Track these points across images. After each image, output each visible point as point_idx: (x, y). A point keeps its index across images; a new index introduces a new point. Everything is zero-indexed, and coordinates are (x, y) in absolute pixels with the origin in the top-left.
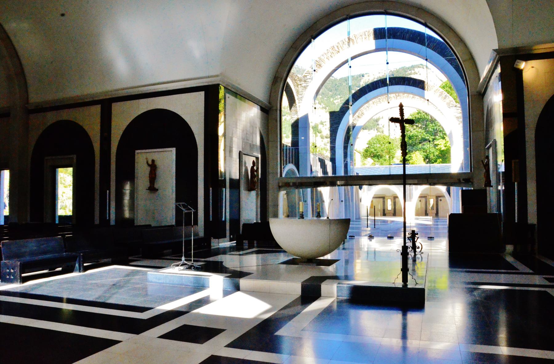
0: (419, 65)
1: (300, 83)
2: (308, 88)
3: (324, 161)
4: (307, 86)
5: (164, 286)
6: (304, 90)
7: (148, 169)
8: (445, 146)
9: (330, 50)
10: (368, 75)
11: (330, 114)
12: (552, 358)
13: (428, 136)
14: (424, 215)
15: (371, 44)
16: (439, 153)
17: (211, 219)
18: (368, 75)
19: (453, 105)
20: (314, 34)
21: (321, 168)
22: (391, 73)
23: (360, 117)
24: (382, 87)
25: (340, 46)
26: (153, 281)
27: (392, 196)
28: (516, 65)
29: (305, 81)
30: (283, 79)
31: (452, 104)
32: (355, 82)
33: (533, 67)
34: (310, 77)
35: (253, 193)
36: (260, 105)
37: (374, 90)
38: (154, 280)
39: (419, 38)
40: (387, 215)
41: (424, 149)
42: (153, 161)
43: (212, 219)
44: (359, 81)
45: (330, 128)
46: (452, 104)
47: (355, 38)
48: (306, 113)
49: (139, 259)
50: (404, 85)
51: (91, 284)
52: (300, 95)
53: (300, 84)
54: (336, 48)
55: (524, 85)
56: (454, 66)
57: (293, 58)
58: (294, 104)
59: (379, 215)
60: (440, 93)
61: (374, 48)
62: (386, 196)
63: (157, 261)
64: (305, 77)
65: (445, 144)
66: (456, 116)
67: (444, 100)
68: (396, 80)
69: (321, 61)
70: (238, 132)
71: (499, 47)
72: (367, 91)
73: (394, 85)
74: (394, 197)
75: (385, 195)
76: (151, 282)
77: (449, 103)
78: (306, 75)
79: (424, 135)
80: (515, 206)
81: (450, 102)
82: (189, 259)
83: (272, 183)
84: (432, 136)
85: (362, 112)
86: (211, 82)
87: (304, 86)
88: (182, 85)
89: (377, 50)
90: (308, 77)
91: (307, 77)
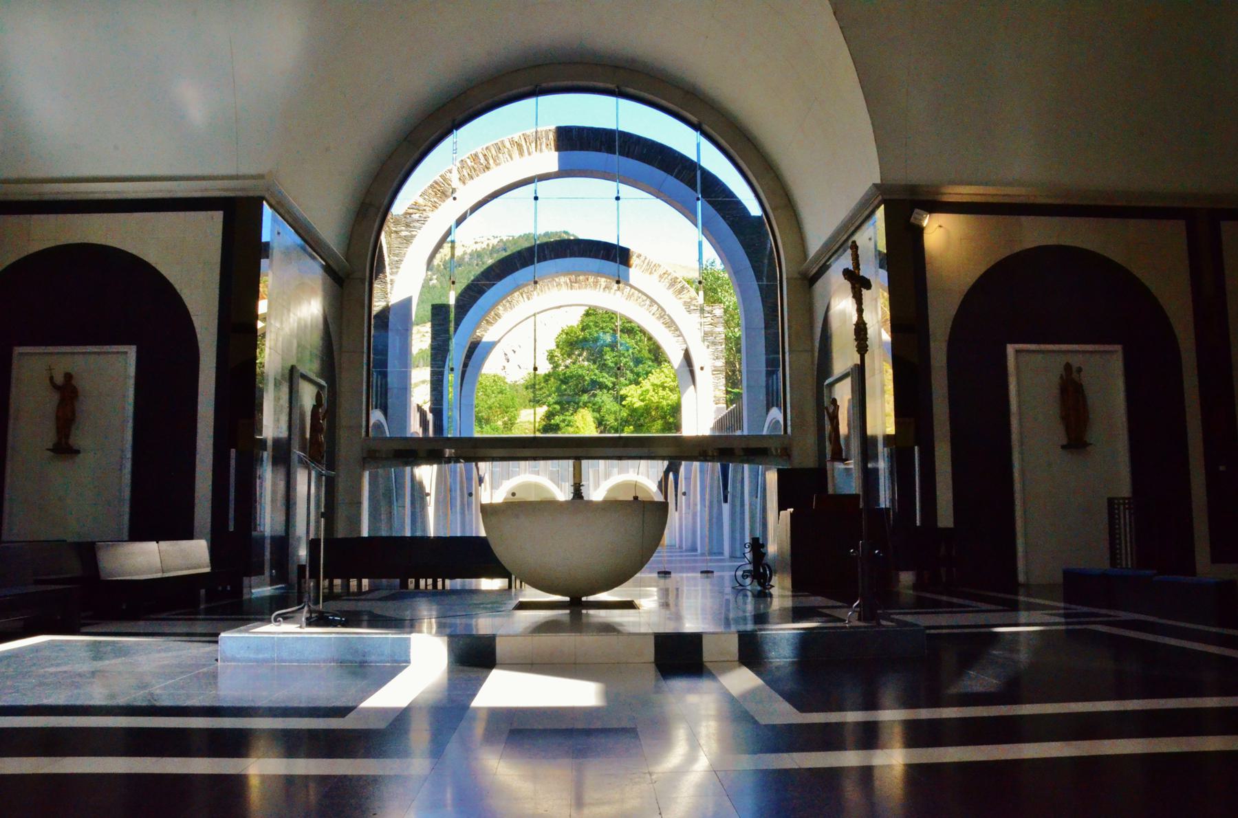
0: (560, 232)
1: (394, 229)
2: (415, 241)
4: (413, 236)
5: (273, 668)
6: (405, 245)
7: (55, 398)
8: (642, 400)
9: (468, 161)
11: (432, 309)
12: (1235, 748)
13: (603, 377)
15: (550, 160)
16: (629, 415)
17: (233, 527)
20: (460, 118)
21: (421, 426)
22: (501, 244)
23: (491, 323)
24: (551, 259)
25: (490, 155)
26: (238, 656)
28: (915, 218)
29: (407, 225)
31: (694, 305)
33: (940, 226)
34: (420, 216)
38: (243, 654)
41: (594, 404)
42: (68, 377)
47: (526, 142)
48: (410, 295)
49: (89, 622)
51: (55, 674)
52: (395, 255)
53: (396, 232)
54: (482, 160)
55: (926, 256)
56: (728, 221)
58: (381, 276)
60: (671, 280)
61: (554, 168)
63: (142, 623)
64: (408, 216)
65: (642, 395)
67: (680, 296)
68: (582, 246)
69: (446, 184)
70: (291, 320)
71: (881, 180)
72: (518, 265)
76: (234, 659)
77: (689, 303)
78: (411, 211)
79: (595, 375)
80: (915, 498)
81: (689, 300)
82: (240, 617)
83: (348, 448)
84: (611, 376)
86: (234, 190)
87: (405, 236)
88: (161, 191)
89: (563, 173)
90: (416, 217)
91: (412, 216)
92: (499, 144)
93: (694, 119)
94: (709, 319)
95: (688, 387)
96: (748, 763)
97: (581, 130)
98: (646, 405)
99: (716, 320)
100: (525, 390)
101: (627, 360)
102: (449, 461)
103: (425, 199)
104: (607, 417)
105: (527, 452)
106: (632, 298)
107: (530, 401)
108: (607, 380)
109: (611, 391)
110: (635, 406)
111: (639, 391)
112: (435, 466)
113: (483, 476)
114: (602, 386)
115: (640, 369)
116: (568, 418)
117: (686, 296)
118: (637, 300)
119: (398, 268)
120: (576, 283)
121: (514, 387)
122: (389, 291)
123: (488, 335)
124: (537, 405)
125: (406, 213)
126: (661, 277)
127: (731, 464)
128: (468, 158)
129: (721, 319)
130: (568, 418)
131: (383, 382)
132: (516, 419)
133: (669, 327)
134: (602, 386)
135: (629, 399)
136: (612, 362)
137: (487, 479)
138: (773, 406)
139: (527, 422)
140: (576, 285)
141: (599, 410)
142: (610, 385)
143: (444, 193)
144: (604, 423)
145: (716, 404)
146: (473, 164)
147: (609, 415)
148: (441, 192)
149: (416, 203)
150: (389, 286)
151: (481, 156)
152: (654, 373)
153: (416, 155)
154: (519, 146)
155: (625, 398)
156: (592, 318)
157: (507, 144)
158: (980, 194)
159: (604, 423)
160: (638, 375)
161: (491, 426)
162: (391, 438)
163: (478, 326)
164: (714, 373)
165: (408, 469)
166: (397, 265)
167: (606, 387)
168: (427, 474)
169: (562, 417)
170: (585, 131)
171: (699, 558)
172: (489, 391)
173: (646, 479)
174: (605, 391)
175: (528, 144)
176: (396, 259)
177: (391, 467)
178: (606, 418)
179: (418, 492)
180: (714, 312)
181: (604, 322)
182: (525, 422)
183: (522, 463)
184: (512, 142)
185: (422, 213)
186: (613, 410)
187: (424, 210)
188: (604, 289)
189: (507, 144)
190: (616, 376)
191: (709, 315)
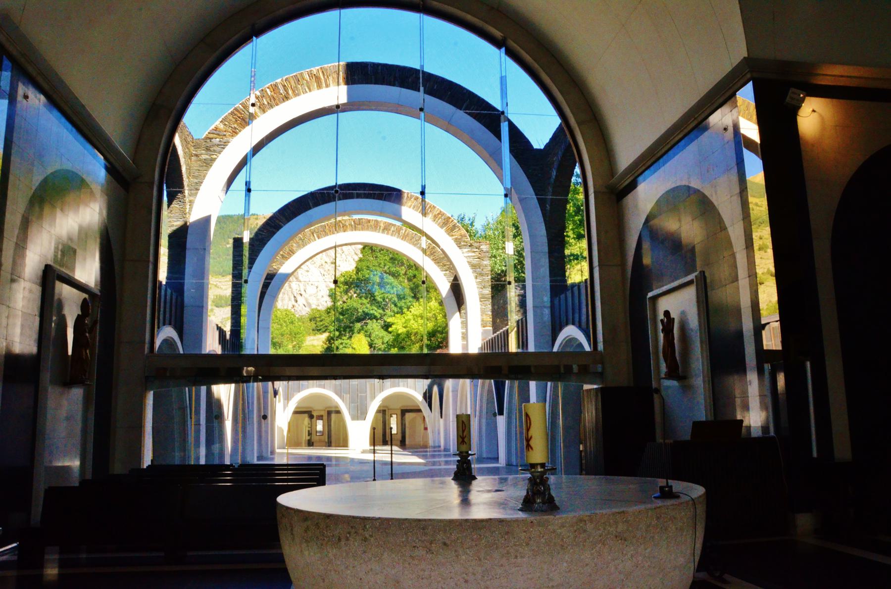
1: (194, 152)
2: (215, 165)
3: (224, 334)
4: (213, 160)
6: (205, 168)
8: (405, 327)
9: (268, 90)
10: (255, 217)
14: (382, 443)
18: (255, 217)
19: (467, 243)
21: (220, 343)
23: (286, 257)
25: (289, 86)
27: (325, 410)
28: (792, 98)
29: (208, 149)
30: (174, 113)
32: (234, 226)
33: (814, 111)
34: (220, 141)
35: (77, 393)
36: (112, 160)
37: (323, 204)
39: (449, 93)
40: (315, 444)
41: (366, 332)
43: (818, 455)
44: (240, 225)
45: (233, 270)
46: (464, 241)
50: (381, 200)
52: (194, 177)
53: (196, 155)
57: (207, 64)
59: (304, 445)
60: (444, 219)
62: (314, 410)
64: (208, 141)
65: (405, 323)
66: (472, 263)
72: (311, 204)
73: (362, 198)
74: (328, 411)
75: (311, 408)
77: (459, 239)
78: (211, 136)
79: (367, 308)
85: (290, 247)
87: (205, 159)
91: (212, 140)
92: (298, 76)
93: (498, 34)
94: (477, 254)
95: (454, 314)
96: (205, 281)
97: (375, 66)
98: (408, 332)
99: (483, 255)
100: (309, 322)
101: (393, 296)
102: (247, 380)
103: (225, 125)
104: (376, 341)
105: (314, 371)
106: (407, 238)
107: (313, 330)
108: (377, 312)
109: (379, 321)
110: (400, 332)
111: (403, 320)
112: (233, 385)
113: (277, 389)
114: (373, 317)
115: (401, 303)
116: (345, 341)
117: (457, 234)
118: (411, 240)
119: (198, 190)
120: (359, 225)
121: (301, 319)
122: (187, 210)
123: (285, 268)
124: (318, 333)
125: (207, 138)
126: (435, 217)
127: (507, 381)
128: (268, 88)
129: (487, 254)
130: (345, 341)
131: (179, 299)
132: (303, 343)
133: (438, 263)
134: (373, 317)
135: (394, 326)
136: (380, 298)
137: (281, 391)
138: (567, 324)
139: (314, 344)
140: (360, 227)
141: (370, 336)
142: (379, 316)
143: (244, 120)
144: (373, 346)
145: (484, 327)
146: (272, 93)
147: (377, 339)
148: (241, 119)
149: (217, 128)
150: (188, 207)
151: (280, 87)
152: (415, 306)
153: (212, 59)
154: (318, 79)
155: (391, 325)
156: (364, 264)
157: (307, 77)
158: (850, 77)
159: (373, 346)
160: (401, 308)
161: (283, 349)
162: (184, 356)
163: (273, 258)
164: (483, 300)
165: (204, 389)
166: (196, 188)
167: (375, 318)
168: (224, 392)
169: (340, 341)
170: (380, 68)
171: (442, 453)
172: (281, 321)
173: (414, 391)
174: (375, 321)
175: (326, 77)
176: (196, 181)
177: (186, 386)
178: (375, 342)
179: (214, 409)
180: (481, 247)
181: (374, 266)
182: (310, 346)
183: (311, 382)
184: (311, 74)
185: (222, 138)
186: (381, 335)
187: (225, 135)
188: (383, 230)
189: (307, 77)
190: (383, 309)
191: (477, 250)
